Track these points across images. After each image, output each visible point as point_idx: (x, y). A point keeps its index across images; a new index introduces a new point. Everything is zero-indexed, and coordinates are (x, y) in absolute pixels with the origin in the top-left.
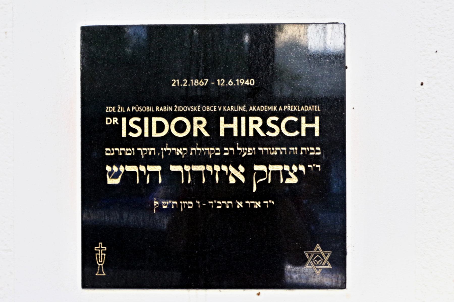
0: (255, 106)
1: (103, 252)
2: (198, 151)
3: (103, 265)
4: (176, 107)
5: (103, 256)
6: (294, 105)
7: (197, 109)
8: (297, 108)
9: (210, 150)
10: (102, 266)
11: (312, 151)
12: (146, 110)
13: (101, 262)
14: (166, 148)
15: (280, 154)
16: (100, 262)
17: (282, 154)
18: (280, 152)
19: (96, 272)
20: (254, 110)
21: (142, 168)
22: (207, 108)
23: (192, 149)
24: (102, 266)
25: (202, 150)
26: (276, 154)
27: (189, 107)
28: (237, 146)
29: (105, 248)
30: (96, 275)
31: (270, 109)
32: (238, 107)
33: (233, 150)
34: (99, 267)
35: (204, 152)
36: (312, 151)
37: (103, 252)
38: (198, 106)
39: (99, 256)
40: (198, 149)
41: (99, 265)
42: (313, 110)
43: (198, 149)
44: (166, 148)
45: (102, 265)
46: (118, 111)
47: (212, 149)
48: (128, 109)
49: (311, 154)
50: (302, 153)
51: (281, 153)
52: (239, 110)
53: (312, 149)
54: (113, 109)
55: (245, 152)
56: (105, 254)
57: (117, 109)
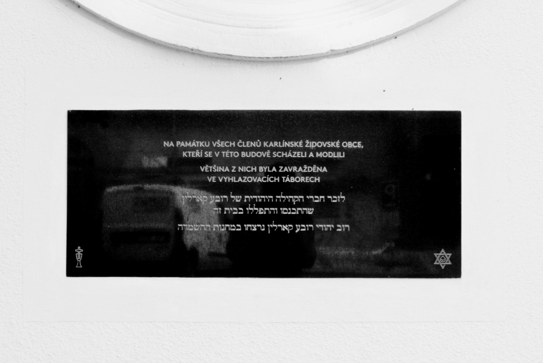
0: (267, 142)
1: (81, 253)
2: (282, 199)
3: (81, 261)
4: (307, 142)
5: (81, 255)
6: (250, 141)
7: (335, 144)
8: (204, 144)
9: (294, 198)
10: (80, 262)
11: (235, 211)
12: (348, 146)
13: (80, 259)
14: (340, 196)
15: (269, 213)
16: (78, 259)
17: (270, 213)
18: (269, 212)
19: (76, 265)
20: (275, 146)
21: (231, 209)
22: (349, 145)
23: (277, 197)
24: (80, 262)
25: (286, 198)
26: (298, 213)
27: (325, 143)
28: (231, 194)
29: (82, 250)
30: (77, 267)
31: (188, 145)
32: (283, 142)
33: (226, 198)
34: (78, 263)
35: (288, 199)
36: (235, 211)
37: (81, 253)
38: (300, 141)
39: (78, 255)
40: (283, 197)
41: (78, 260)
42: (198, 146)
43: (283, 197)
44: (340, 196)
45: (80, 261)
46: (306, 146)
47: (295, 197)
48: (172, 144)
49: (234, 213)
50: (225, 213)
51: (270, 213)
52: (286, 146)
53: (235, 209)
54: (348, 145)
55: (213, 200)
56: (82, 254)
57: (304, 144)
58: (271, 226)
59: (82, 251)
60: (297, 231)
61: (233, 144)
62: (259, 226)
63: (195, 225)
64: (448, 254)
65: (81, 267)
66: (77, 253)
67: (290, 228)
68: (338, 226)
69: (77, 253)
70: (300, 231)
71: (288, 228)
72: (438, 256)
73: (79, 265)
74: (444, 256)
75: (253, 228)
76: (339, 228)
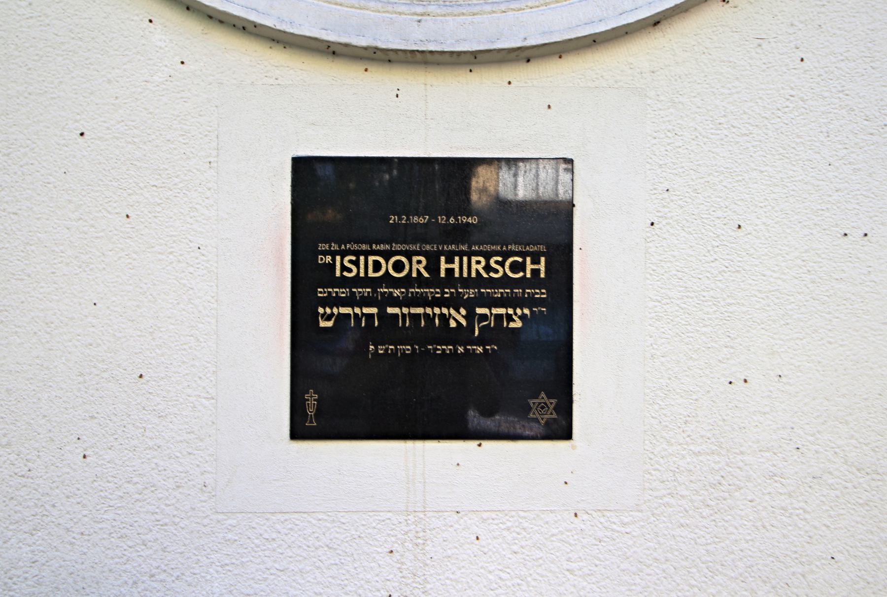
1: (315, 400)
2: (417, 293)
3: (314, 415)
37: (315, 400)
40: (417, 290)
43: (417, 290)
45: (312, 414)
58: (382, 290)
59: (316, 396)
60: (465, 298)
61: (417, 267)
62: (330, 290)
63: (519, 311)
64: (552, 401)
65: (315, 424)
66: (308, 400)
67: (403, 293)
68: (446, 290)
69: (308, 400)
70: (469, 297)
71: (400, 292)
72: (542, 419)
73: (311, 422)
74: (545, 403)
75: (510, 318)
76: (447, 293)
